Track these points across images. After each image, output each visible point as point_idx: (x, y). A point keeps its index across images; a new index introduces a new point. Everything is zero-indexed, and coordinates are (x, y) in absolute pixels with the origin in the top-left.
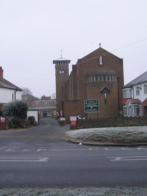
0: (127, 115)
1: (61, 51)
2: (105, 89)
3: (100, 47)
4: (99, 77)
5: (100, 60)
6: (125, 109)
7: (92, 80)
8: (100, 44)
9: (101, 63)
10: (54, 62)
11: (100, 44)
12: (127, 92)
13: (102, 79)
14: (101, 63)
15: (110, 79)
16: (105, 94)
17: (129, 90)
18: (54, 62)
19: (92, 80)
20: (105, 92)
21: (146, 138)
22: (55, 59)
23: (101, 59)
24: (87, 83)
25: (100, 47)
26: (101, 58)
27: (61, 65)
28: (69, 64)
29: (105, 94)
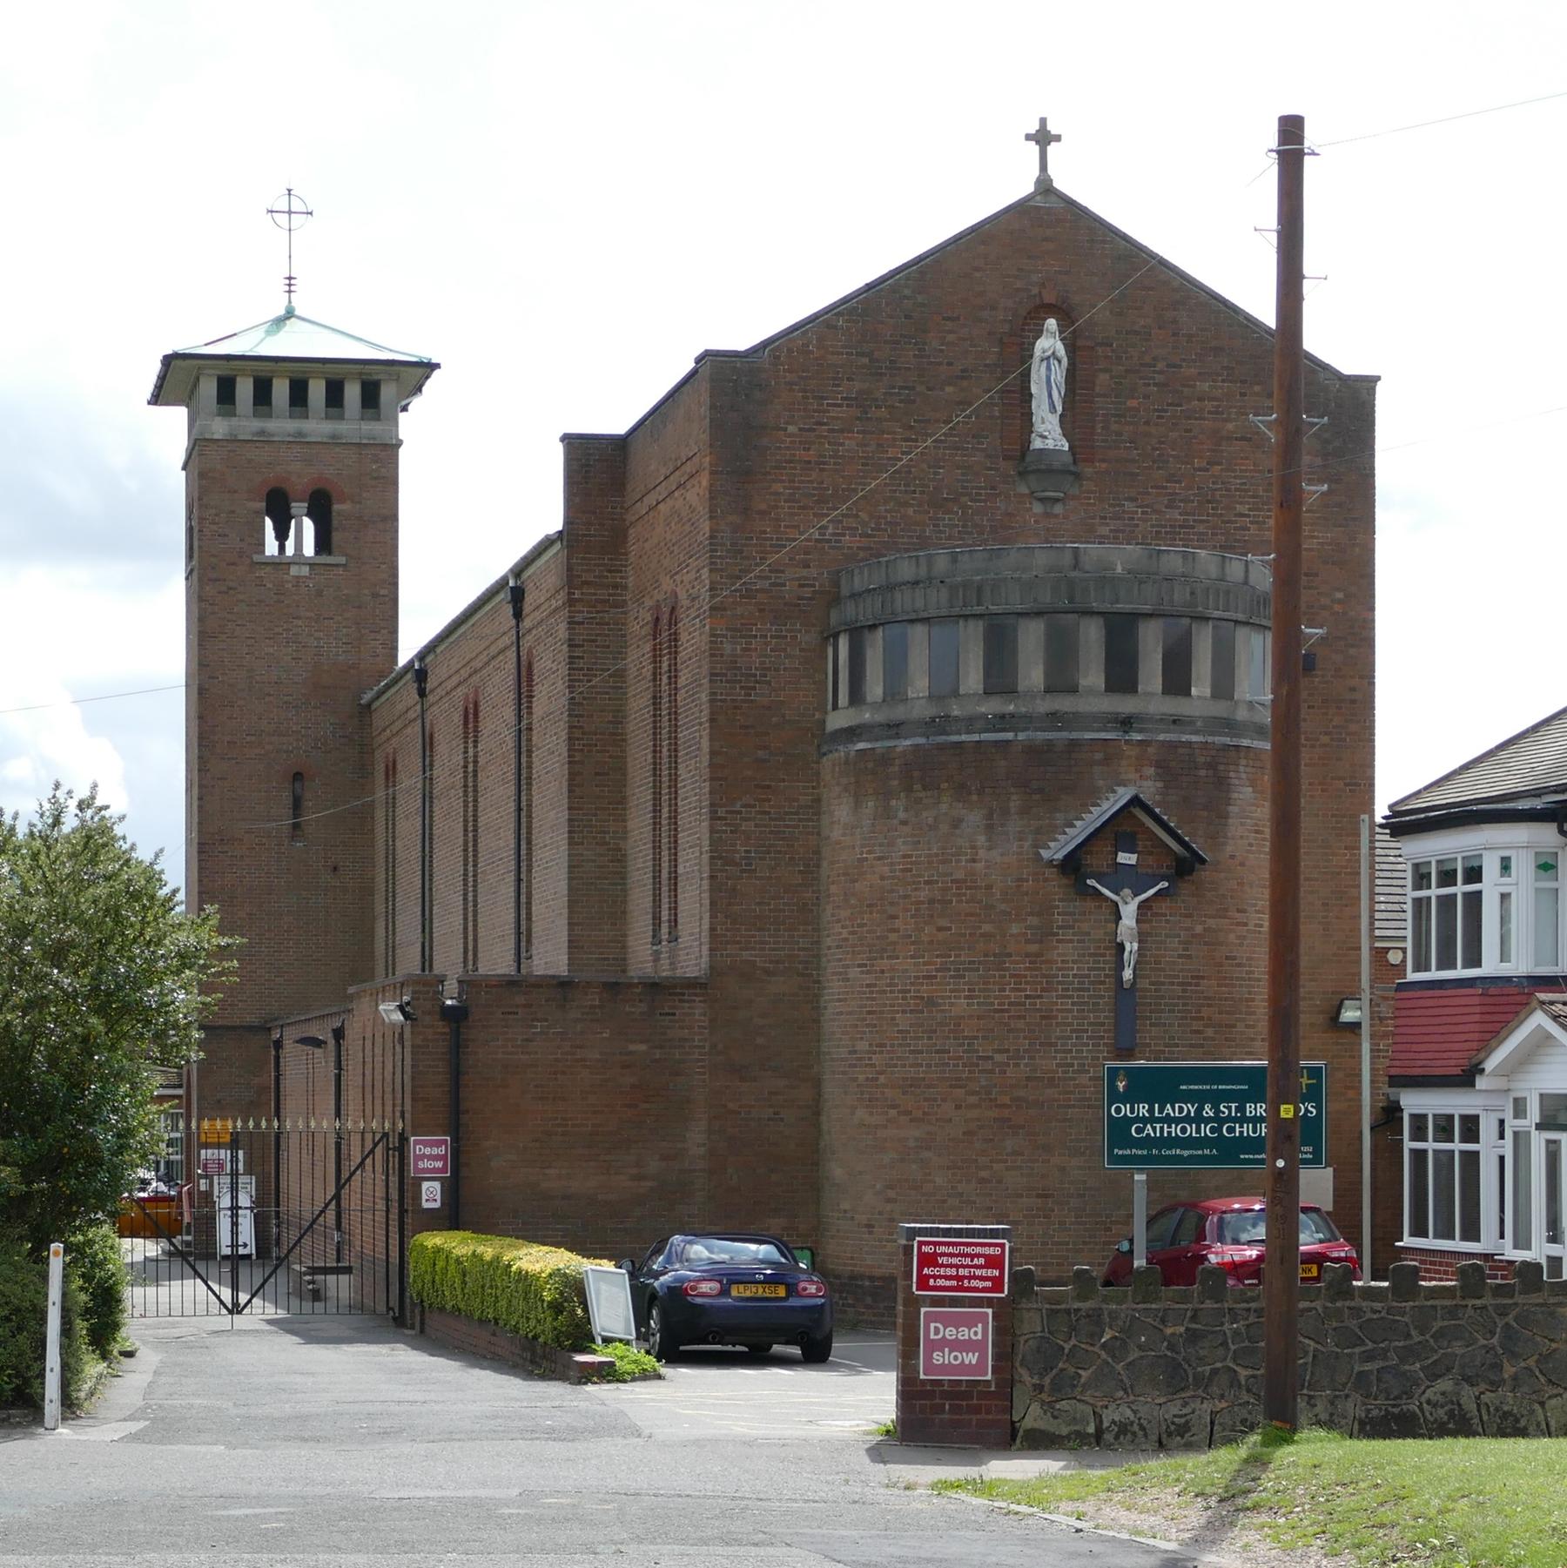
0: (1472, 1232)
1: (289, 210)
2: (1119, 830)
3: (1045, 186)
4: (1031, 638)
5: (1038, 374)
6: (1430, 1145)
7: (919, 685)
8: (1043, 138)
9: (1048, 432)
10: (179, 378)
11: (1043, 138)
12: (1490, 886)
13: (1093, 676)
14: (1048, 432)
15: (1201, 688)
16: (1129, 911)
17: (1523, 866)
18: (179, 378)
19: (919, 685)
20: (1135, 880)
21: (4, 1420)
22: (197, 335)
23: (1059, 374)
24: (837, 721)
25: (1045, 186)
26: (1049, 342)
27: (288, 450)
28: (402, 416)
29: (1129, 911)
